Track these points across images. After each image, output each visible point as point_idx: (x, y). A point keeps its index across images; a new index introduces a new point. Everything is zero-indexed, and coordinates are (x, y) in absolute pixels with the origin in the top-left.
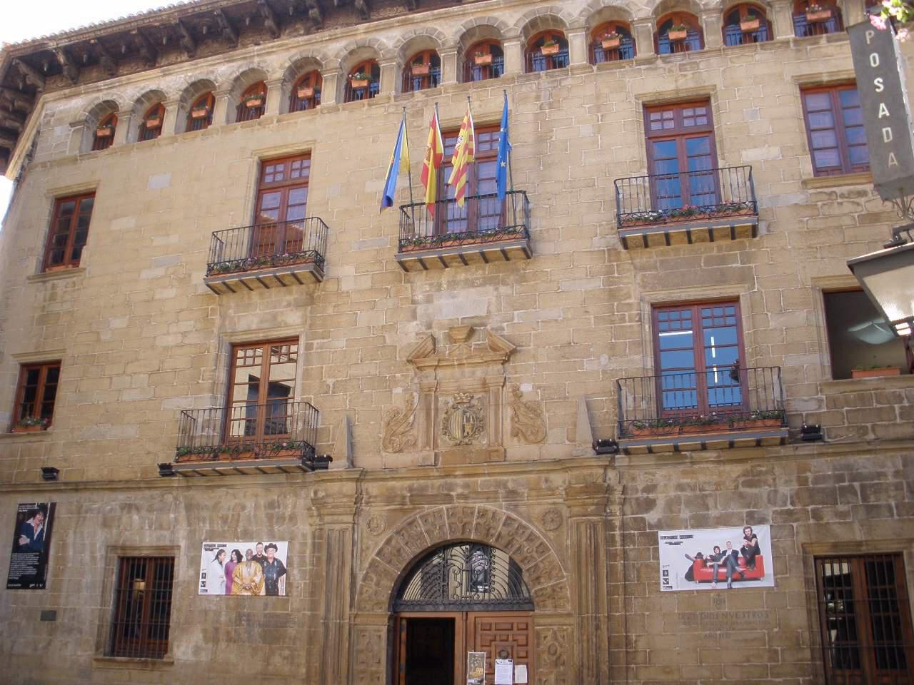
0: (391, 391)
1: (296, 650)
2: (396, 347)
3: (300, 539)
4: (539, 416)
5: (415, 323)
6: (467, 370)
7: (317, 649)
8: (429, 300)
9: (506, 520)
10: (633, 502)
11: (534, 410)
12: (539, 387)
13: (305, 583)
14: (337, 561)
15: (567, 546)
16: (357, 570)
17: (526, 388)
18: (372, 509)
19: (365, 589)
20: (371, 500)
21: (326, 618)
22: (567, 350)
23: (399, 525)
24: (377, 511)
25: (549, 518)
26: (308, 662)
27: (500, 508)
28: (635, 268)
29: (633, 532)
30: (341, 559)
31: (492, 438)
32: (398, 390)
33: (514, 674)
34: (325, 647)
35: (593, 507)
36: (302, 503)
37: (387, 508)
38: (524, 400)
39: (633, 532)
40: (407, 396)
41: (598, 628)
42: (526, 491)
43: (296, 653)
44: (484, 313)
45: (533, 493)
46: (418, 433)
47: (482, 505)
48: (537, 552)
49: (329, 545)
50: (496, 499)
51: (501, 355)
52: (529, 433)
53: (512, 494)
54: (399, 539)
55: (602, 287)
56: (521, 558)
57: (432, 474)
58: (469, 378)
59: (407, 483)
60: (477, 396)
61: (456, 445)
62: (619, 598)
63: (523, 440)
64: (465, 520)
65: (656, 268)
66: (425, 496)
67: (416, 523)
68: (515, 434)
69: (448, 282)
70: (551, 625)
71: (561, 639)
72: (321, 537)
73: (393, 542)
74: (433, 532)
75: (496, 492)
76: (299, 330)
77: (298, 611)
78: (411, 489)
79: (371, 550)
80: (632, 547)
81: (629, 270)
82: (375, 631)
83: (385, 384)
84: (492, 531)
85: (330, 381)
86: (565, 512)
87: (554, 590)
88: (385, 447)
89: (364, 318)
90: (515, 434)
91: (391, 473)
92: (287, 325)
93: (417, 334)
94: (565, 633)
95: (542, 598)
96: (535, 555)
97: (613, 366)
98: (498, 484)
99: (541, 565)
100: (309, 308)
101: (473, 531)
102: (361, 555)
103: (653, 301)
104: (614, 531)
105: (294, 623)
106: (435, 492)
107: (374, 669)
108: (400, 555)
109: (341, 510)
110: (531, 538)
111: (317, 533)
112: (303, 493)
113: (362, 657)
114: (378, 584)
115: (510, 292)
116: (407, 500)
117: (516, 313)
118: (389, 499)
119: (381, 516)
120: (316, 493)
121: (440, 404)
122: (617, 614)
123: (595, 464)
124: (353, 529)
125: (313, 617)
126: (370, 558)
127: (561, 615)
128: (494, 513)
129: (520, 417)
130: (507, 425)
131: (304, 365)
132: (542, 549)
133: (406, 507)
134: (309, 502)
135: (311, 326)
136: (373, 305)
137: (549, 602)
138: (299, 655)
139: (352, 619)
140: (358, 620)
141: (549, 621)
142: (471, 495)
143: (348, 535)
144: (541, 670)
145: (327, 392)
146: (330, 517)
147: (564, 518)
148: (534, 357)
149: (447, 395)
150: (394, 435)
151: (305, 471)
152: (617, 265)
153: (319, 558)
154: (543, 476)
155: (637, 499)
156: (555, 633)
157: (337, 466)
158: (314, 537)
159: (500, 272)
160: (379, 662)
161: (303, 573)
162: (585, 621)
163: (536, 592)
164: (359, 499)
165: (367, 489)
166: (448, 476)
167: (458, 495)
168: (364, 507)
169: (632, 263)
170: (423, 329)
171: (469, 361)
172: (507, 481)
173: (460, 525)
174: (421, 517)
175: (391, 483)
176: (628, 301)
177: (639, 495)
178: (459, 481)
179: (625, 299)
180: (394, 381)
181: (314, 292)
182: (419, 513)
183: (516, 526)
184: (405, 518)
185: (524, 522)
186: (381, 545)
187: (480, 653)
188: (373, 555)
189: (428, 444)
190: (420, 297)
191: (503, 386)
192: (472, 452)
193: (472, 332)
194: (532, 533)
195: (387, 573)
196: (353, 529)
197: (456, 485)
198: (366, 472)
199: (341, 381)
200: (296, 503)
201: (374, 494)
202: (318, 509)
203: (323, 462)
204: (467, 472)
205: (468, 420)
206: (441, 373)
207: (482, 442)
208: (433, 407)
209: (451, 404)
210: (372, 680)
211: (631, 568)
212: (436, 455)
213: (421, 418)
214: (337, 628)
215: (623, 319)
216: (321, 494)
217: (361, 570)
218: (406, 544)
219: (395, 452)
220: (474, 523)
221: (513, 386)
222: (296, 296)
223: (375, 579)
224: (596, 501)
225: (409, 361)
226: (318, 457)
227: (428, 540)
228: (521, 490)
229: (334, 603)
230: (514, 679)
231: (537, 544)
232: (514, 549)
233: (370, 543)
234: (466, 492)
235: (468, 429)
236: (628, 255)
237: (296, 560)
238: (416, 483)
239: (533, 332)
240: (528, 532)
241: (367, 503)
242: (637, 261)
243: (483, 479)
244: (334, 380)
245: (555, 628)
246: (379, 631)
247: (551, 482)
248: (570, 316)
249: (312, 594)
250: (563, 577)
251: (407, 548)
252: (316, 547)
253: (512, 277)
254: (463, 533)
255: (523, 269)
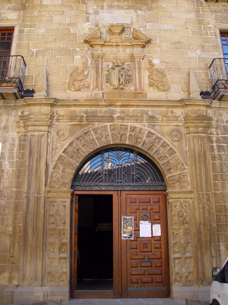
0: (73, 57)
1: (5, 215)
2: (77, 34)
3: (10, 141)
4: (165, 76)
5: (88, 23)
6: (121, 49)
7: (21, 214)
8: (97, 13)
9: (148, 134)
10: (222, 128)
11: (161, 73)
12: (164, 62)
13: (13, 170)
14: (36, 155)
15: (186, 151)
16: (49, 162)
17: (156, 61)
18: (60, 124)
19: (55, 174)
20: (60, 118)
21: (28, 193)
22: (177, 45)
23: (78, 133)
24: (64, 125)
25: (174, 133)
26: (14, 223)
27: (144, 126)
28: (211, 11)
29: (223, 144)
30: (39, 154)
31: (138, 86)
32: (78, 57)
33: (152, 230)
34: (27, 213)
35: (201, 129)
36: (12, 118)
37: (70, 123)
38: (155, 67)
39: (223, 144)
40: (83, 61)
41: (208, 200)
42: (160, 117)
43: (5, 217)
44: (129, 22)
45: (165, 119)
46: (91, 80)
47: (133, 124)
48: (168, 153)
49: (30, 145)
50: (141, 121)
51: (143, 42)
52: (160, 85)
53: (152, 118)
54: (78, 143)
55: (194, 17)
56: (158, 157)
57: (101, 104)
58: (123, 53)
59: (84, 109)
60: (126, 64)
61: (115, 89)
62: (219, 183)
63: (156, 89)
64: (122, 133)
65: (222, 12)
66: (96, 116)
67: (89, 133)
68: (151, 85)
69: (108, 5)
70: (179, 198)
71: (184, 207)
72: (25, 140)
73: (74, 145)
74: (101, 139)
75: (142, 117)
76: (15, 23)
77: (8, 188)
78: (86, 112)
79: (58, 150)
80: (223, 153)
81: (208, 12)
82: (61, 202)
83: (71, 54)
84: (139, 140)
85: (35, 50)
86: (183, 130)
87: (180, 178)
88: (69, 88)
89: (57, 19)
90: (151, 85)
91: (76, 103)
92: (7, 20)
93: (89, 29)
94: (187, 204)
95: (172, 182)
96: (167, 155)
97: (204, 56)
98: (143, 112)
99: (171, 162)
100: (22, 12)
101: (127, 139)
102: (52, 152)
103: (221, 28)
104: (213, 143)
105: (5, 196)
106: (102, 115)
107: (61, 227)
108: (79, 153)
109: (41, 123)
110: (164, 145)
111: (22, 138)
112: (14, 113)
113: (52, 219)
114: (63, 171)
115: (144, 14)
116: (84, 118)
117: (148, 24)
118: (72, 117)
119: (66, 128)
120: (22, 113)
121: (104, 66)
122: (218, 192)
123: (202, 104)
124: (48, 135)
125: (18, 193)
126: (59, 155)
127: (185, 192)
128: (141, 129)
129: (154, 76)
130: (146, 80)
131: (18, 41)
132: (172, 152)
133: (83, 123)
134: (18, 119)
135: (23, 20)
136: (63, 13)
137: (177, 184)
138: (8, 218)
139: (46, 194)
140: (50, 195)
141: (177, 196)
142: (126, 118)
143: (44, 139)
144: (174, 227)
145: (32, 56)
146: (32, 127)
147: (183, 135)
148: (159, 46)
149: (109, 61)
150: (75, 79)
151: (17, 98)
152: (202, 9)
153: (23, 154)
154: (170, 109)
155: (224, 126)
156: (181, 204)
157: (39, 95)
158: (20, 140)
159: (138, 4)
160: (64, 223)
161: (12, 163)
162: (201, 196)
163: (169, 177)
164: (52, 117)
165: (57, 111)
166: (111, 105)
167: (118, 117)
168: (54, 122)
169: (209, 9)
170: (93, 27)
171: (123, 44)
172: (148, 111)
173: (119, 136)
174: (93, 130)
175: (73, 109)
176: (209, 26)
177: (225, 124)
178: (118, 109)
179: (207, 25)
180: (76, 53)
181: (25, 4)
182: (92, 127)
183: (155, 138)
184: (82, 130)
185: (159, 136)
186: (66, 146)
187: (130, 217)
188: (61, 152)
189: (97, 87)
190: (91, 11)
191: (143, 59)
192: (125, 93)
193: (123, 31)
194: (164, 142)
195: (70, 164)
196: (48, 135)
197: (116, 111)
198: (58, 100)
199: (42, 50)
200: (8, 120)
201: (62, 114)
202: (24, 122)
203: (30, 93)
204: (123, 104)
205: (122, 76)
206: (105, 49)
207: (131, 88)
208: (100, 66)
209: (111, 66)
210: (60, 235)
211: (224, 165)
212: (103, 93)
213: (93, 72)
214: (36, 199)
215: (207, 34)
216: (26, 113)
217: (52, 162)
218: (83, 146)
219: (76, 91)
220: (128, 134)
221: (149, 60)
222: (14, 5)
223: (61, 168)
224: (204, 124)
225: (86, 42)
226: (26, 90)
227: (98, 144)
228: (157, 116)
229: (33, 183)
230: (152, 233)
231: (168, 149)
232: (154, 151)
233: (58, 145)
234: (123, 115)
235: (122, 80)
236: (207, 5)
237: (7, 155)
238: (90, 109)
239: (158, 34)
240: (162, 142)
241: (57, 120)
242: (212, 8)
243: (133, 109)
244: (37, 50)
245: (182, 200)
246: (64, 202)
247: (175, 113)
248: (178, 29)
249: (18, 177)
250: (185, 169)
251: (83, 149)
252: (21, 147)
253: (145, 7)
254: (120, 141)
255: (150, 4)
